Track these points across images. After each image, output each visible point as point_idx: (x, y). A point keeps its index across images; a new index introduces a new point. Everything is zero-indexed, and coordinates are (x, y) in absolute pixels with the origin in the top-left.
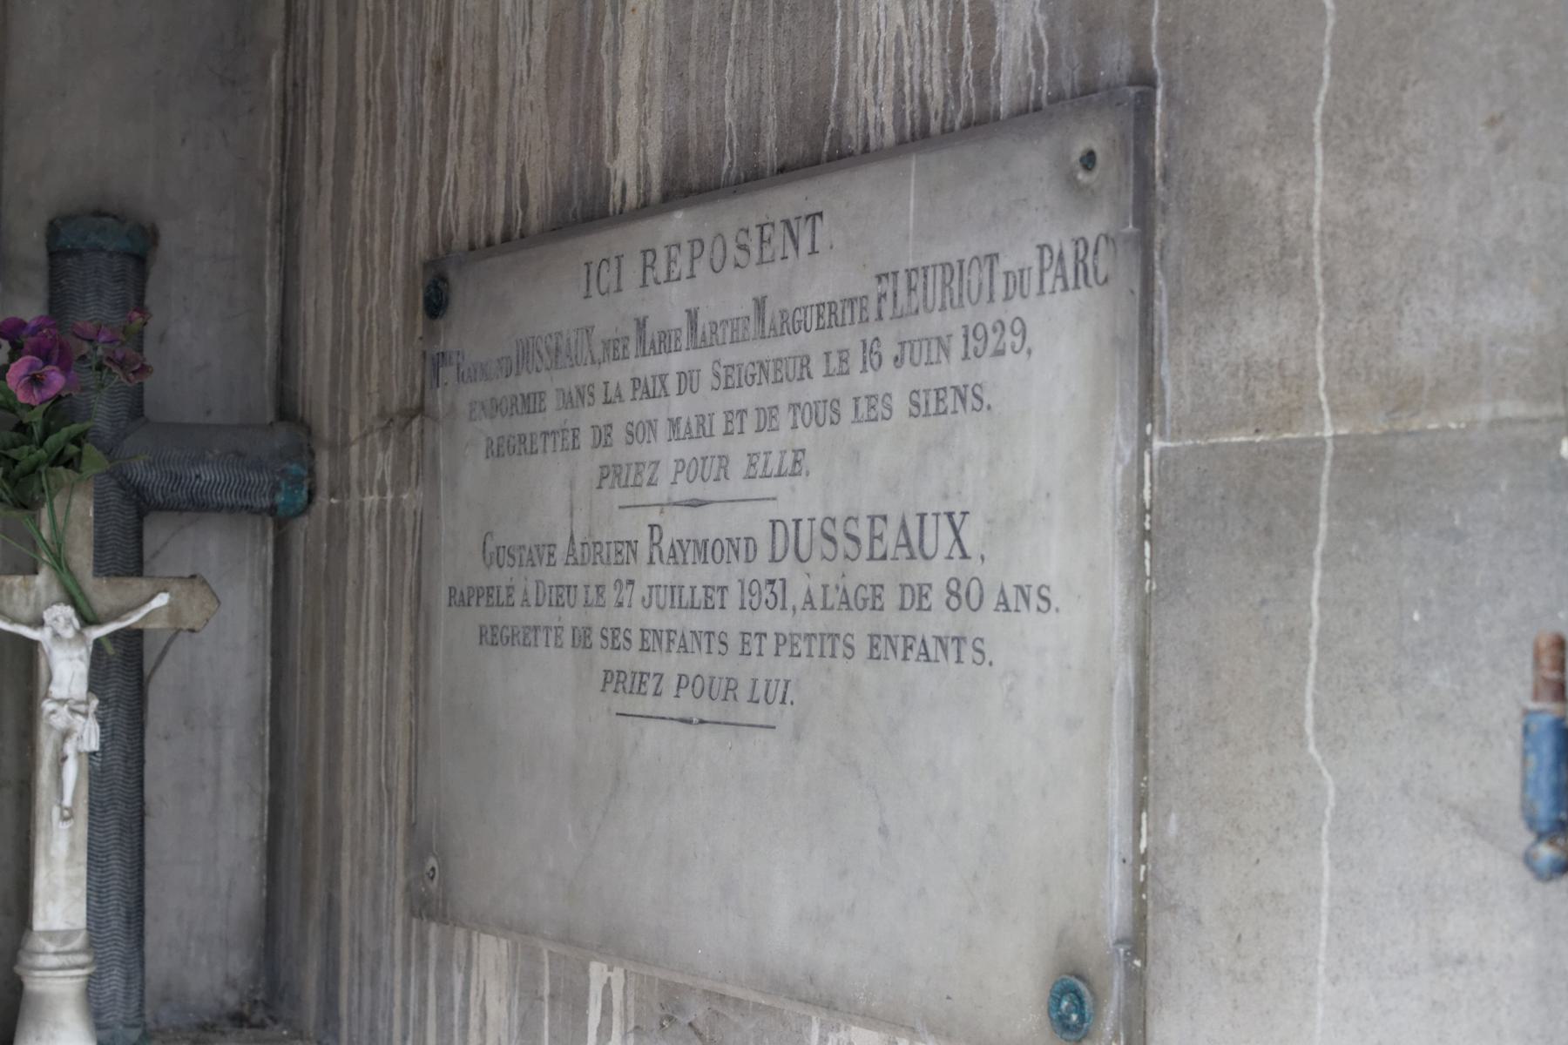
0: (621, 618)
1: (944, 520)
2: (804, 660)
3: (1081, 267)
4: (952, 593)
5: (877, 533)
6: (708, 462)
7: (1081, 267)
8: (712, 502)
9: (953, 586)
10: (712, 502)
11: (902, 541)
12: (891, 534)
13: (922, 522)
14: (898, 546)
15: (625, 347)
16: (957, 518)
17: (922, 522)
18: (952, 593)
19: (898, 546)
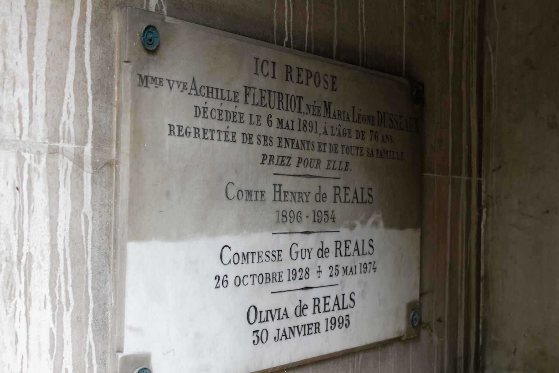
0: (332, 157)
1: (307, 250)
2: (232, 89)
3: (281, 103)
4: (284, 216)
5: (327, 302)
6: (313, 161)
7: (281, 103)
8: (300, 289)
9: (284, 213)
10: (300, 289)
11: (193, 87)
12: (352, 246)
13: (228, 93)
14: (192, 89)
15: (319, 111)
16: (310, 250)
17: (228, 93)
18: (284, 216)
19: (192, 89)
